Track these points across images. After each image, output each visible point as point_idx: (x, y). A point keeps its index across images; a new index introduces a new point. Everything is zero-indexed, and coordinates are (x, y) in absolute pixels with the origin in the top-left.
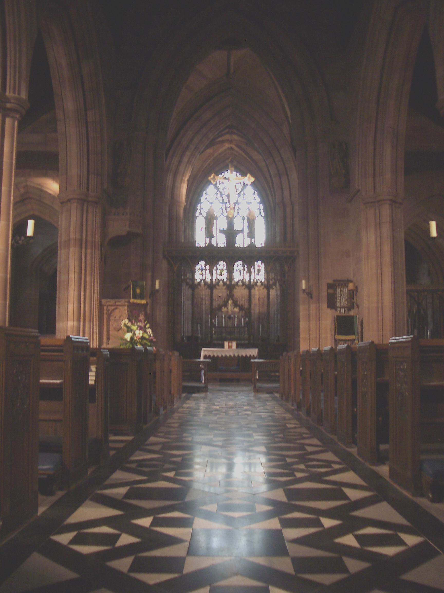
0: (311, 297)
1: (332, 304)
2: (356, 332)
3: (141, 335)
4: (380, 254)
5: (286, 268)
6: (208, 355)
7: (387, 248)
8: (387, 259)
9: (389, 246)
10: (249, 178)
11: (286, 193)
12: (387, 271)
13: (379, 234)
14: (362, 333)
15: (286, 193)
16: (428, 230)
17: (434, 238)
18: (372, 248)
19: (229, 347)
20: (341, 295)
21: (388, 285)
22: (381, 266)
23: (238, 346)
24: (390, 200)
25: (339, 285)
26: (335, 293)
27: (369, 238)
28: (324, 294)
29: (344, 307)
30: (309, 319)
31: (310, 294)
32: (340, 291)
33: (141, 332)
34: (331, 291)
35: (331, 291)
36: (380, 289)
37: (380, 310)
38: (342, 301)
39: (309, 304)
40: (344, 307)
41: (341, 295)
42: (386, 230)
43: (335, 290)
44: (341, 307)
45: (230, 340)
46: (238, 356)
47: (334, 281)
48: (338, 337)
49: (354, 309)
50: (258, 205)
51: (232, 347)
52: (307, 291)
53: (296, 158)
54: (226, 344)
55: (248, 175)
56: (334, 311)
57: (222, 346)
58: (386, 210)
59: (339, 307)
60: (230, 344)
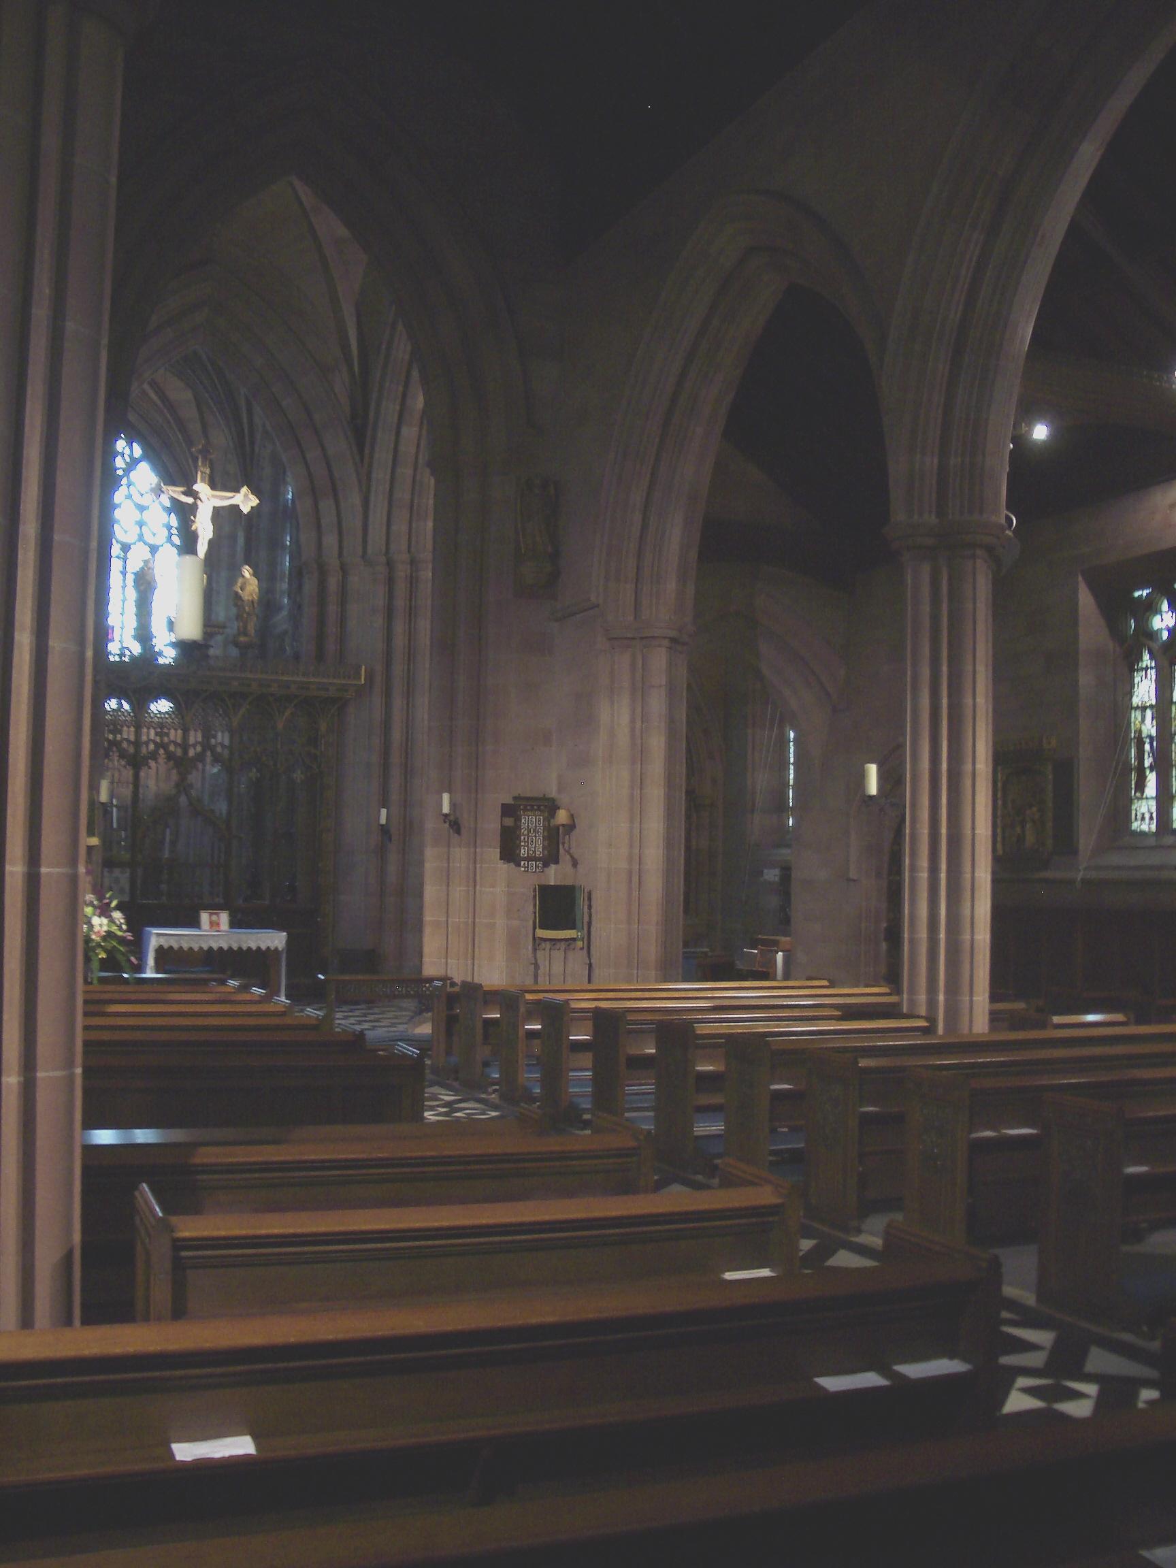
0: (458, 832)
1: (509, 853)
2: (579, 924)
3: (105, 928)
4: (639, 754)
5: (323, 727)
6: (166, 946)
7: (657, 743)
8: (657, 767)
9: (663, 739)
10: (246, 496)
11: (330, 540)
12: (656, 794)
13: (639, 710)
14: (590, 924)
15: (330, 540)
16: (862, 777)
17: (871, 797)
18: (623, 738)
19: (212, 924)
20: (529, 831)
21: (655, 825)
22: (640, 782)
23: (234, 924)
24: (673, 640)
25: (525, 810)
26: (517, 827)
27: (616, 717)
28: (492, 824)
29: (536, 859)
30: (447, 877)
31: (455, 825)
32: (531, 822)
33: (105, 921)
34: (509, 822)
35: (509, 822)
36: (637, 831)
37: (635, 879)
38: (531, 844)
39: (449, 846)
40: (536, 859)
41: (529, 831)
42: (657, 703)
43: (518, 820)
44: (528, 859)
45: (215, 907)
46: (240, 948)
47: (515, 798)
48: (541, 933)
49: (557, 862)
50: (165, 515)
51: (218, 924)
52: (452, 818)
53: (362, 460)
54: (204, 917)
55: (244, 489)
56: (512, 865)
57: (195, 924)
58: (659, 659)
59: (525, 859)
60: (214, 918)
